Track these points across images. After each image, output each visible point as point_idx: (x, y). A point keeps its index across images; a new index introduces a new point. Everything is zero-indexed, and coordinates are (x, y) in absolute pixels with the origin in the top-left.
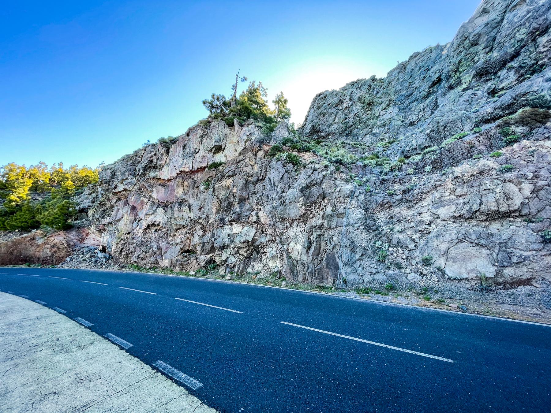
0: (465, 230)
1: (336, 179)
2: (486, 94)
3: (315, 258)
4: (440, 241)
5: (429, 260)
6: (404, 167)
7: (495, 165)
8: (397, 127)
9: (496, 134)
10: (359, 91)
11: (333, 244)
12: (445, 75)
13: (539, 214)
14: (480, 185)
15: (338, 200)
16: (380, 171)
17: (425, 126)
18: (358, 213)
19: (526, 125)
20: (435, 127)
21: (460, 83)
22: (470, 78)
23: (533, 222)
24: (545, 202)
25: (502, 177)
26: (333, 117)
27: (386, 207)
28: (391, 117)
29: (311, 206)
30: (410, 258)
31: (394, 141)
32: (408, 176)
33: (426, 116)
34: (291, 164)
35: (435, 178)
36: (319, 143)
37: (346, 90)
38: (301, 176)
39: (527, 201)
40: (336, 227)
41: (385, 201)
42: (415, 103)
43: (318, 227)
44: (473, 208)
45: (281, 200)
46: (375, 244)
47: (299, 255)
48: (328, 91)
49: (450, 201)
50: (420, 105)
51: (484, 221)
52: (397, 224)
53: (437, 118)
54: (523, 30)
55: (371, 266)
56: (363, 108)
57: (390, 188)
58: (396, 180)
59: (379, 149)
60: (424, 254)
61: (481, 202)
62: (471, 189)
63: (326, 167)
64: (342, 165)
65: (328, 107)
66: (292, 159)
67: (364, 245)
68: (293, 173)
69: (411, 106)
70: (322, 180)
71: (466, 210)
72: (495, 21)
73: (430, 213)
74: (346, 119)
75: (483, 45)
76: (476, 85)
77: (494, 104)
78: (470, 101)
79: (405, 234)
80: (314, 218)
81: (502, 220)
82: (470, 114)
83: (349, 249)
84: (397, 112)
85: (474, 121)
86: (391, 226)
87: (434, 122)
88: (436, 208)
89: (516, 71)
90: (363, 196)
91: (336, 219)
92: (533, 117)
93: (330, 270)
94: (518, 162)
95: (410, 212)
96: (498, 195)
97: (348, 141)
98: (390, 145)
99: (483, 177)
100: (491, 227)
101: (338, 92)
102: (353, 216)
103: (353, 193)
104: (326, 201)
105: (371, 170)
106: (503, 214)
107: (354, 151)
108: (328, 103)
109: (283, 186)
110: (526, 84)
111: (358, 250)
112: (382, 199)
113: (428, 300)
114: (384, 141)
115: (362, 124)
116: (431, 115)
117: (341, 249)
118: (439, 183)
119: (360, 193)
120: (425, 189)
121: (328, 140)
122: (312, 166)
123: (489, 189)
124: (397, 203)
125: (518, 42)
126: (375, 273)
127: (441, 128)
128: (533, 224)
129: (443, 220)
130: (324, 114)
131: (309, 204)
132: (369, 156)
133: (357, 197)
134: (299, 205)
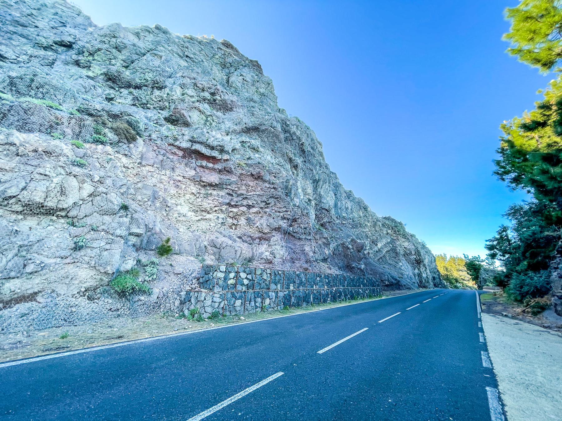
2: (104, 96)
7: (70, 154)
13: (85, 218)
20: (28, 77)
22: (99, 73)
24: (96, 208)
25: (69, 168)
39: (81, 202)
54: (151, 75)
62: (22, 166)
69: (14, 36)
75: (124, 57)
78: (87, 90)
81: (42, 217)
89: (133, 99)
92: (125, 132)
94: (94, 162)
96: (53, 185)
99: (47, 159)
100: (22, 223)
106: (46, 210)
123: (46, 175)
125: (145, 79)
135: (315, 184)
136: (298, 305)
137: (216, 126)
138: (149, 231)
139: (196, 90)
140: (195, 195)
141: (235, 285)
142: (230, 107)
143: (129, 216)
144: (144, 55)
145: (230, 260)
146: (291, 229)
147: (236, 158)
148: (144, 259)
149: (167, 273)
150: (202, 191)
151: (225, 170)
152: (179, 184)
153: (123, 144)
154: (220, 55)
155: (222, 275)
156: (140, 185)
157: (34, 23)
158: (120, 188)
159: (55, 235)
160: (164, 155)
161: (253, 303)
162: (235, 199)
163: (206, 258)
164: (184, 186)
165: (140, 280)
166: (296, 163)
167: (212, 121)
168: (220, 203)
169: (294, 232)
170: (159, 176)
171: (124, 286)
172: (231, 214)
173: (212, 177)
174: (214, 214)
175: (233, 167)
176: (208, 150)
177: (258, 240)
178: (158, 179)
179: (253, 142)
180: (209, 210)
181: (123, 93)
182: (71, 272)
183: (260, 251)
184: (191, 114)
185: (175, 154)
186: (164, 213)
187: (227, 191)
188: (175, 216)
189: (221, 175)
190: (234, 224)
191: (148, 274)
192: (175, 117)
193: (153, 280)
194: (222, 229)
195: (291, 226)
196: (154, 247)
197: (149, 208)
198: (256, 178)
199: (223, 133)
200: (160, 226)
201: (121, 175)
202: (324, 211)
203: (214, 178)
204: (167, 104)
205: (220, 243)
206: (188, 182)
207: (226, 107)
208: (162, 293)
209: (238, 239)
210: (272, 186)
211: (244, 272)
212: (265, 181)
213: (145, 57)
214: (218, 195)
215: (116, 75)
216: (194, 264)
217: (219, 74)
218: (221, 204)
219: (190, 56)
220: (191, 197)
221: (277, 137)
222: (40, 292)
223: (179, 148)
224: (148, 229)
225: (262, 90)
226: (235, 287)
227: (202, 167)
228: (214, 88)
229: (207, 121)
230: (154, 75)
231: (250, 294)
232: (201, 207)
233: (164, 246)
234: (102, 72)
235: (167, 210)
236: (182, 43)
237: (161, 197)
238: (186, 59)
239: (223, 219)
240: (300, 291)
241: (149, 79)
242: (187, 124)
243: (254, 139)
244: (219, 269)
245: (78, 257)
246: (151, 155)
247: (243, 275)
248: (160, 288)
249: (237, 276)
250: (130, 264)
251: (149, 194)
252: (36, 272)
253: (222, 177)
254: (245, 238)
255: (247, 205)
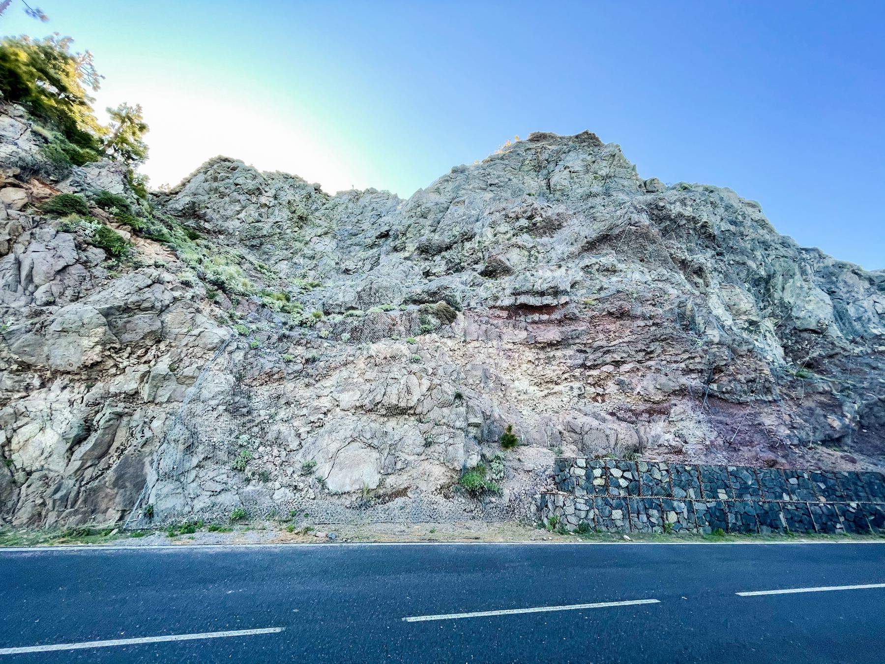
1: (198, 311)
2: (421, 272)
3: (89, 464)
5: (312, 467)
6: (319, 325)
8: (327, 268)
11: (148, 434)
14: (389, 371)
15: (190, 351)
16: (283, 320)
17: (358, 281)
26: (238, 208)
29: (120, 349)
31: (318, 285)
32: (320, 340)
33: (364, 269)
34: (101, 250)
35: (349, 351)
36: (193, 237)
37: (273, 179)
38: (117, 282)
40: (168, 401)
41: (275, 370)
42: (357, 248)
43: (123, 396)
44: (377, 398)
45: (35, 320)
47: (43, 457)
48: (242, 162)
54: (458, 228)
55: (217, 479)
56: (291, 220)
57: (291, 351)
58: (302, 341)
59: (295, 288)
60: (308, 457)
63: (187, 284)
65: (233, 187)
66: (108, 241)
67: (215, 439)
68: (98, 271)
69: (352, 249)
70: (168, 306)
74: (258, 222)
79: (291, 425)
80: (121, 376)
83: (181, 447)
86: (273, 410)
88: (339, 392)
90: (242, 353)
91: (172, 385)
93: (122, 491)
96: (401, 386)
98: (311, 289)
101: (259, 174)
103: (224, 345)
104: (162, 346)
105: (271, 315)
108: (236, 182)
109: (56, 290)
111: (201, 448)
112: (271, 365)
113: (291, 531)
114: (306, 280)
115: (281, 242)
117: (165, 445)
118: (351, 358)
119: (238, 348)
120: (334, 363)
121: (215, 240)
122: (155, 273)
124: (293, 376)
126: (220, 492)
127: (373, 291)
130: (222, 196)
131: (117, 346)
132: (275, 293)
133: (231, 353)
134: (86, 342)
135: (763, 285)
136: (747, 529)
137: (544, 258)
141: (605, 488)
142: (558, 223)
143: (465, 405)
145: (600, 450)
146: (714, 386)
148: (489, 454)
150: (542, 355)
152: (510, 353)
154: (530, 158)
159: (410, 433)
160: (487, 323)
161: (644, 518)
162: (591, 357)
163: (563, 448)
166: (696, 266)
167: (536, 254)
168: (570, 367)
169: (723, 393)
170: (486, 350)
172: (590, 380)
173: (550, 333)
174: (565, 384)
175: (576, 311)
176: (537, 298)
177: (645, 415)
179: (603, 260)
183: (653, 433)
184: (508, 256)
186: (500, 394)
187: (575, 347)
189: (563, 326)
190: (598, 394)
193: (502, 478)
194: (581, 405)
195: (709, 381)
197: (482, 391)
198: (617, 317)
201: (449, 360)
202: (805, 335)
203: (553, 334)
204: (480, 254)
205: (580, 425)
207: (552, 227)
208: (513, 495)
209: (609, 417)
211: (617, 467)
212: (635, 318)
213: (449, 211)
214: (565, 356)
217: (534, 183)
218: (572, 368)
221: (646, 236)
223: (502, 308)
224: (486, 417)
225: (603, 172)
226: (607, 490)
228: (530, 209)
229: (530, 256)
231: (635, 501)
232: (544, 377)
233: (507, 435)
236: (482, 171)
238: (491, 188)
239: (580, 388)
240: (747, 504)
241: (457, 234)
242: (507, 271)
243: (603, 256)
245: (430, 453)
246: (474, 327)
247: (617, 473)
249: (606, 473)
250: (474, 460)
253: (564, 329)
254: (621, 414)
255: (613, 362)
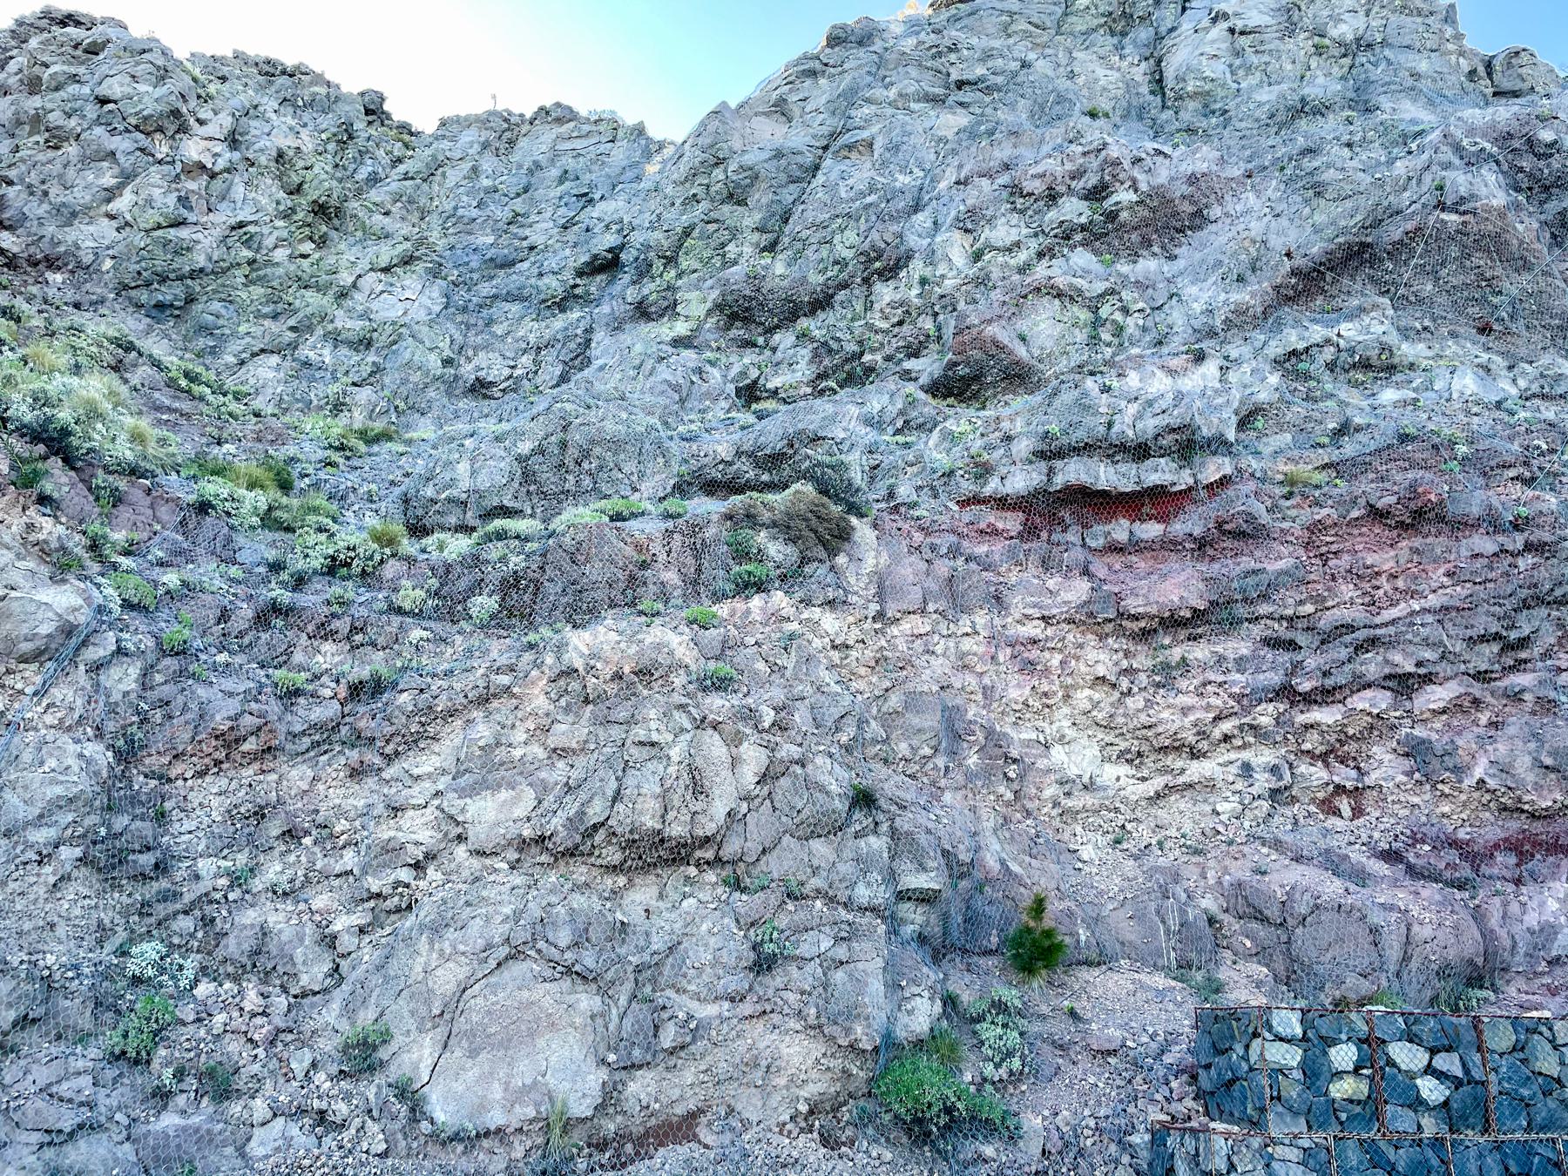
0: (544, 903)
4: (442, 951)
5: (375, 1048)
6: (391, 569)
8: (416, 377)
9: (717, 541)
10: (290, 121)
12: (635, 253)
14: (631, 721)
16: (271, 555)
18: (71, 762)
19: (793, 541)
21: (670, 309)
23: (744, 890)
24: (784, 819)
25: (697, 706)
26: (109, 180)
27: (244, 755)
28: (406, 319)
30: (290, 1037)
31: (385, 436)
32: (396, 620)
33: (539, 380)
35: (494, 654)
39: (744, 807)
41: (248, 721)
42: (515, 308)
44: (590, 812)
46: (125, 954)
49: (523, 769)
50: (528, 324)
51: (614, 869)
52: (276, 852)
53: (568, 406)
54: (851, 236)
55: (64, 1089)
56: (287, 215)
57: (298, 657)
58: (336, 624)
59: (307, 447)
61: (618, 792)
62: (601, 731)
64: (69, 461)
65: (92, 111)
67: (50, 959)
71: (564, 816)
72: (799, 159)
73: (437, 813)
74: (179, 223)
76: (714, 345)
77: (740, 433)
79: (302, 906)
81: (665, 872)
82: (671, 438)
84: (437, 309)
85: (675, 468)
86: (242, 859)
87: (554, 422)
89: (816, 355)
90: (134, 671)
92: (814, 521)
95: (357, 797)
96: (672, 770)
97: (156, 347)
98: (363, 448)
99: (645, 692)
102: (37, 776)
103: (74, 641)
105: (229, 540)
107: (170, 410)
108: (103, 91)
110: (824, 406)
112: (233, 706)
114: (343, 419)
115: (258, 291)
116: (558, 385)
118: (504, 680)
119: (120, 651)
120: (444, 697)
121: (34, 289)
123: (653, 744)
124: (306, 741)
126: (72, 1134)
127: (573, 452)
128: (744, 897)
129: (478, 853)
130: (56, 139)
132: (241, 465)
133: (96, 668)
137: (1144, 329)
138: (962, 876)
139: (1022, 212)
140: (1114, 686)
141: (1371, 1108)
143: (884, 827)
144: (817, 168)
145: (1351, 980)
147: (1267, 451)
149: (1061, 1047)
151: (1224, 532)
152: (1034, 654)
153: (816, 564)
155: (1291, 1057)
156: (895, 700)
157: (526, 238)
158: (838, 730)
159: (704, 927)
162: (1311, 662)
163: (1223, 974)
164: (1058, 657)
165: (968, 1077)
167: (1118, 316)
171: (916, 1100)
172: (1311, 742)
175: (1259, 509)
176: (1122, 468)
178: (952, 658)
179: (1349, 331)
180: (1192, 739)
181: (781, 347)
182: (762, 1045)
183: (1532, 919)
184: (1022, 325)
185: (994, 532)
186: (1001, 789)
187: (1257, 630)
188: (1048, 793)
189: (1213, 559)
190: (1340, 789)
191: (990, 1053)
192: (968, 364)
193: (1016, 1077)
194: (1280, 825)
196: (994, 940)
198: (1402, 525)
199: (1175, 363)
200: (998, 847)
204: (928, 324)
206: (1070, 637)
208: (1055, 1135)
209: (1380, 868)
210: (1519, 540)
211: (1412, 1038)
212: (1461, 526)
213: (820, 178)
215: (748, 292)
216: (1171, 1007)
218: (1248, 700)
219: (971, 77)
220: (1097, 696)
221: (1496, 245)
222: (701, 1111)
223: (1002, 503)
224: (957, 869)
226: (1377, 1115)
227: (1115, 549)
229: (1097, 323)
230: (863, 228)
231: (1473, 1152)
233: (1029, 930)
234: (709, 305)
235: (1012, 775)
237: (977, 728)
238: (961, 96)
239: (1274, 770)
241: (848, 254)
242: (1019, 377)
243: (1350, 317)
244: (1270, 1029)
246: (909, 569)
247: (1407, 1056)
248: (1046, 1113)
250: (921, 1016)
251: (932, 728)
252: (682, 1048)
